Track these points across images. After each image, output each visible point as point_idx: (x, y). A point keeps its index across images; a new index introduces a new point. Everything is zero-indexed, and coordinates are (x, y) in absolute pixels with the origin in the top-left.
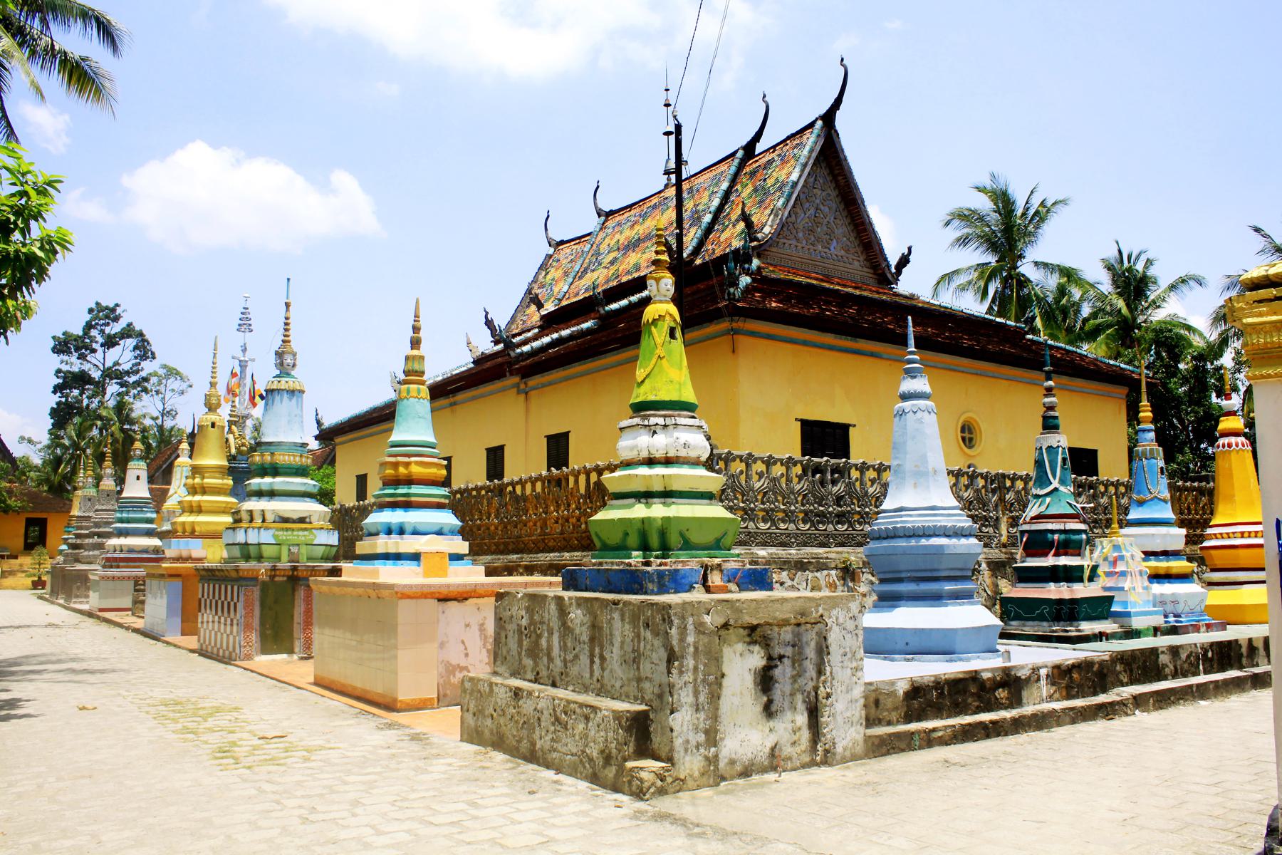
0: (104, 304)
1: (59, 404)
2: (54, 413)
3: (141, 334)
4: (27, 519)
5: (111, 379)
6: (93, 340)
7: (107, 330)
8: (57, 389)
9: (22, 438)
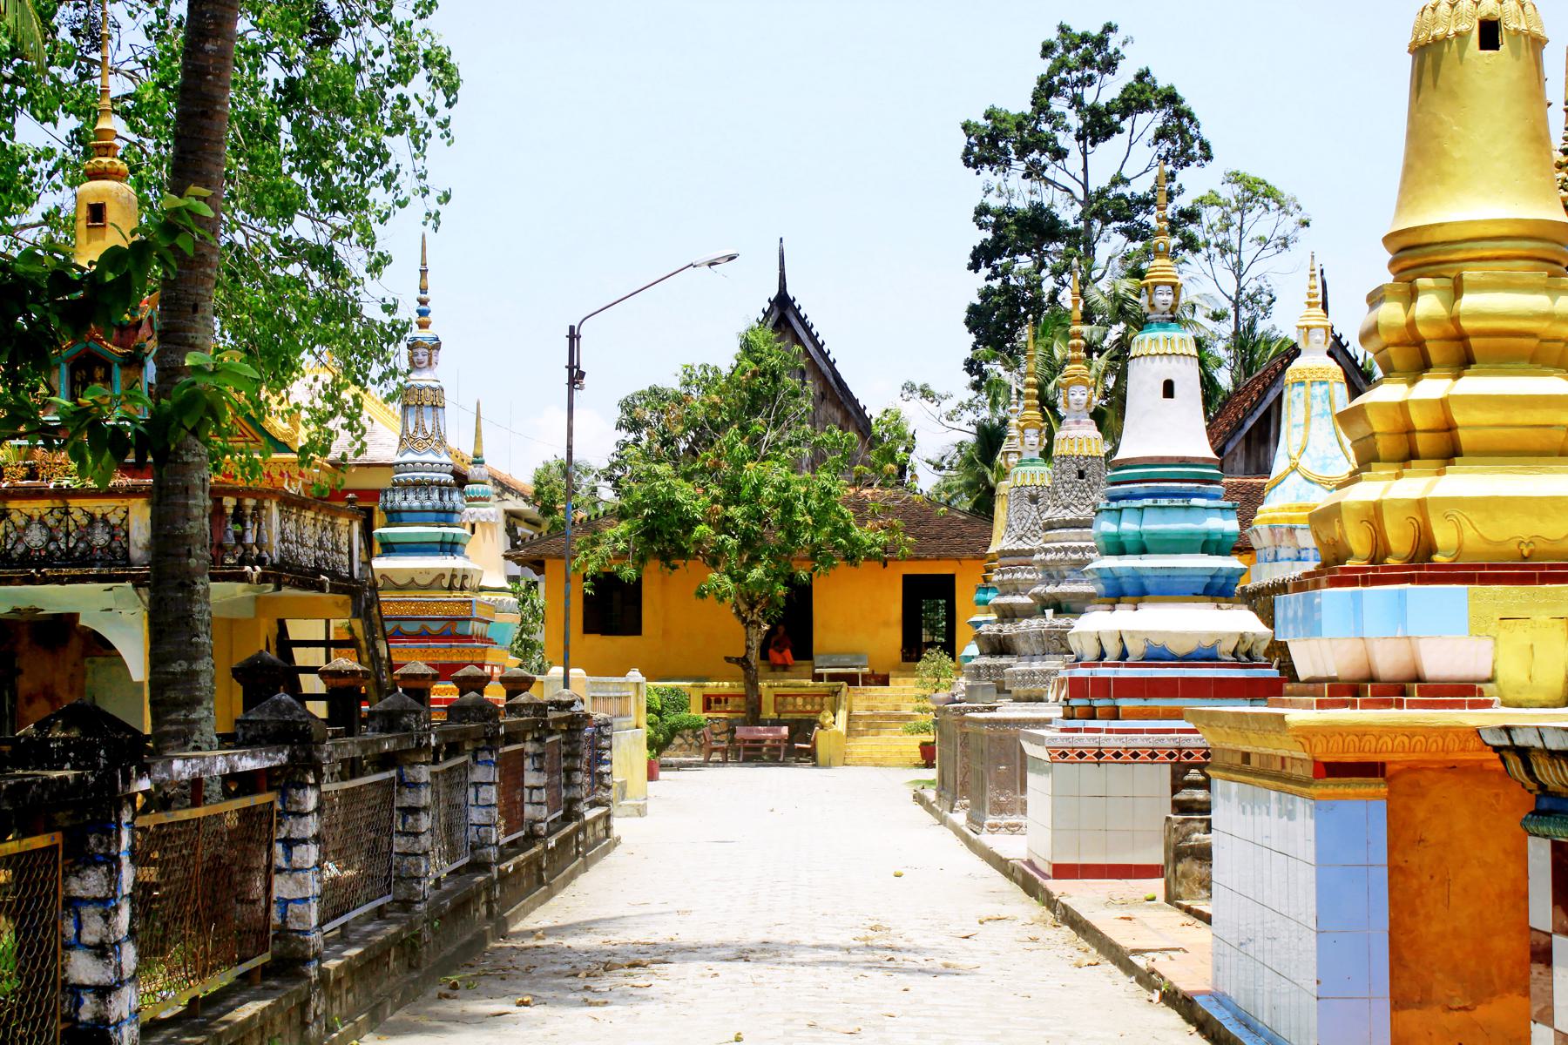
0: (1078, 30)
1: (986, 294)
2: (977, 318)
3: (1171, 98)
4: (907, 579)
5: (1106, 222)
6: (1056, 120)
7: (1089, 95)
8: (982, 255)
9: (911, 388)
